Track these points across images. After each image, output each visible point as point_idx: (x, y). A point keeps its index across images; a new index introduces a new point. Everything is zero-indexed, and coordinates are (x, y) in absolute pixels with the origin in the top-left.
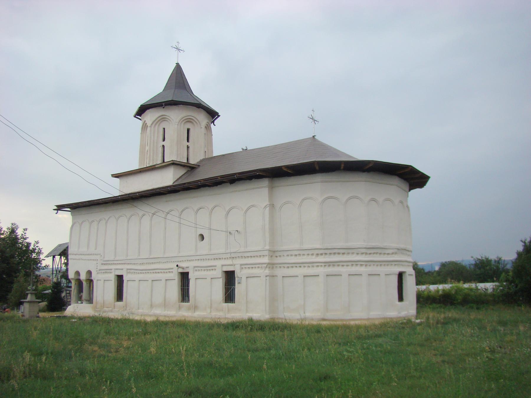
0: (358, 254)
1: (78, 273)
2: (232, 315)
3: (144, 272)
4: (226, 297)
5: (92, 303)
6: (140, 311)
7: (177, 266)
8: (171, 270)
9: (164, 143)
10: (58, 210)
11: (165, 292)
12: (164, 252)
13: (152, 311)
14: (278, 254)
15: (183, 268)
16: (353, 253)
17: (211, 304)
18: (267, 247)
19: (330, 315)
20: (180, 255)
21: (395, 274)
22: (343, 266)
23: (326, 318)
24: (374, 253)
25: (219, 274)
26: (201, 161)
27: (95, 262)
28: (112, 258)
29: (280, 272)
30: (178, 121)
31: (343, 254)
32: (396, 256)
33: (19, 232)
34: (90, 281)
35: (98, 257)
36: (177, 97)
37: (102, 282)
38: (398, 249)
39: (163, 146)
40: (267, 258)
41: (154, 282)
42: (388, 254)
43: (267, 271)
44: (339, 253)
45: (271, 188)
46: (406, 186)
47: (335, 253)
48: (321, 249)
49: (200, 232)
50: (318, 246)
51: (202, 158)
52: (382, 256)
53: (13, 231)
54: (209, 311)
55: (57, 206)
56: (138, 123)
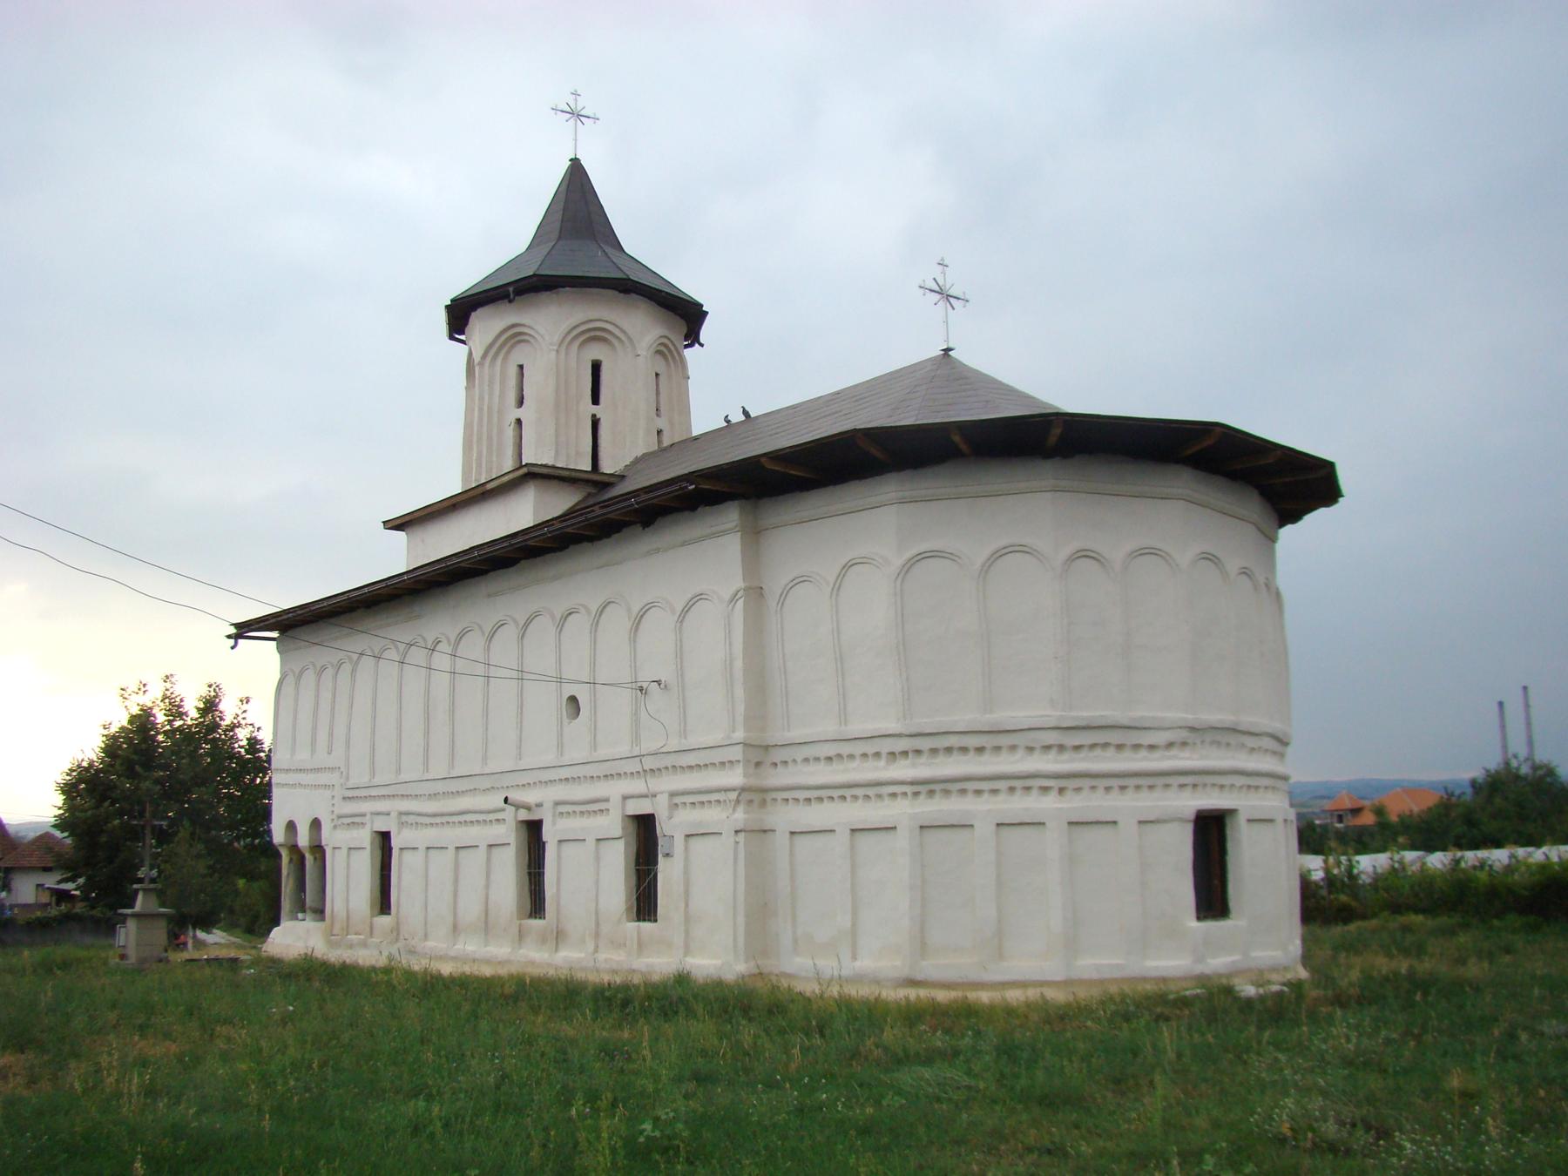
0: (1030, 749)
1: (291, 827)
2: (650, 960)
3: (438, 820)
4: (638, 899)
5: (323, 919)
6: (430, 944)
7: (506, 800)
8: (357, 820)
9: (519, 413)
10: (237, 637)
11: (487, 886)
12: (485, 759)
13: (459, 946)
14: (778, 755)
15: (528, 808)
16: (1013, 748)
17: (598, 924)
18: (739, 735)
19: (931, 968)
20: (523, 765)
21: (1182, 820)
22: (978, 792)
23: (919, 977)
24: (1093, 746)
25: (612, 824)
26: (637, 461)
27: (328, 793)
28: (364, 780)
29: (785, 817)
30: (557, 338)
31: (980, 750)
32: (1186, 753)
33: (228, 710)
34: (318, 850)
35: (332, 778)
36: (577, 264)
37: (345, 851)
38: (1192, 729)
39: (519, 422)
40: (739, 770)
41: (463, 853)
42: (1152, 747)
43: (740, 816)
44: (964, 750)
45: (754, 535)
46: (1252, 506)
47: (949, 750)
48: (900, 735)
49: (569, 690)
50: (893, 726)
51: (640, 452)
52: (1127, 753)
53: (210, 706)
54: (591, 947)
55: (237, 625)
56: (457, 353)
